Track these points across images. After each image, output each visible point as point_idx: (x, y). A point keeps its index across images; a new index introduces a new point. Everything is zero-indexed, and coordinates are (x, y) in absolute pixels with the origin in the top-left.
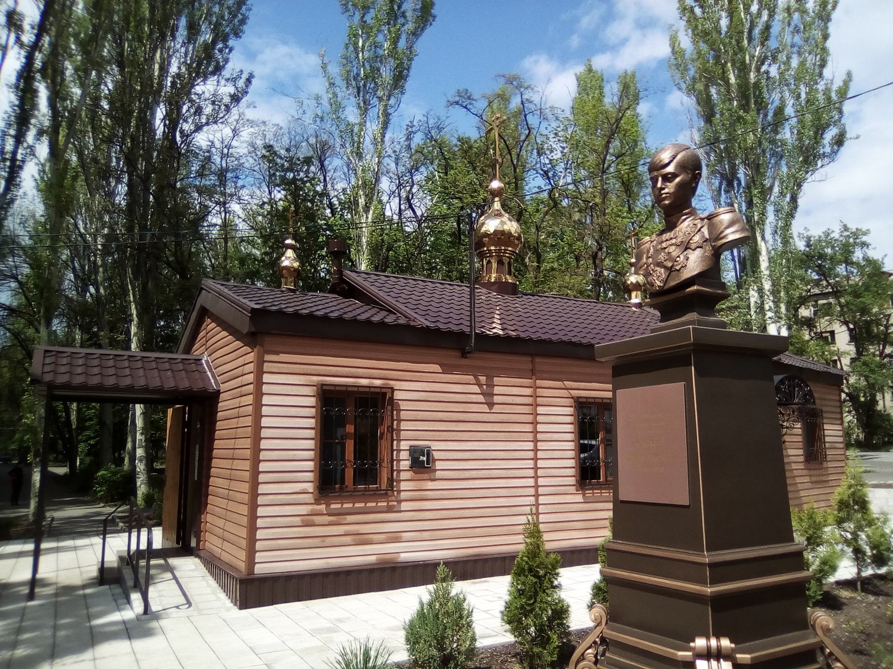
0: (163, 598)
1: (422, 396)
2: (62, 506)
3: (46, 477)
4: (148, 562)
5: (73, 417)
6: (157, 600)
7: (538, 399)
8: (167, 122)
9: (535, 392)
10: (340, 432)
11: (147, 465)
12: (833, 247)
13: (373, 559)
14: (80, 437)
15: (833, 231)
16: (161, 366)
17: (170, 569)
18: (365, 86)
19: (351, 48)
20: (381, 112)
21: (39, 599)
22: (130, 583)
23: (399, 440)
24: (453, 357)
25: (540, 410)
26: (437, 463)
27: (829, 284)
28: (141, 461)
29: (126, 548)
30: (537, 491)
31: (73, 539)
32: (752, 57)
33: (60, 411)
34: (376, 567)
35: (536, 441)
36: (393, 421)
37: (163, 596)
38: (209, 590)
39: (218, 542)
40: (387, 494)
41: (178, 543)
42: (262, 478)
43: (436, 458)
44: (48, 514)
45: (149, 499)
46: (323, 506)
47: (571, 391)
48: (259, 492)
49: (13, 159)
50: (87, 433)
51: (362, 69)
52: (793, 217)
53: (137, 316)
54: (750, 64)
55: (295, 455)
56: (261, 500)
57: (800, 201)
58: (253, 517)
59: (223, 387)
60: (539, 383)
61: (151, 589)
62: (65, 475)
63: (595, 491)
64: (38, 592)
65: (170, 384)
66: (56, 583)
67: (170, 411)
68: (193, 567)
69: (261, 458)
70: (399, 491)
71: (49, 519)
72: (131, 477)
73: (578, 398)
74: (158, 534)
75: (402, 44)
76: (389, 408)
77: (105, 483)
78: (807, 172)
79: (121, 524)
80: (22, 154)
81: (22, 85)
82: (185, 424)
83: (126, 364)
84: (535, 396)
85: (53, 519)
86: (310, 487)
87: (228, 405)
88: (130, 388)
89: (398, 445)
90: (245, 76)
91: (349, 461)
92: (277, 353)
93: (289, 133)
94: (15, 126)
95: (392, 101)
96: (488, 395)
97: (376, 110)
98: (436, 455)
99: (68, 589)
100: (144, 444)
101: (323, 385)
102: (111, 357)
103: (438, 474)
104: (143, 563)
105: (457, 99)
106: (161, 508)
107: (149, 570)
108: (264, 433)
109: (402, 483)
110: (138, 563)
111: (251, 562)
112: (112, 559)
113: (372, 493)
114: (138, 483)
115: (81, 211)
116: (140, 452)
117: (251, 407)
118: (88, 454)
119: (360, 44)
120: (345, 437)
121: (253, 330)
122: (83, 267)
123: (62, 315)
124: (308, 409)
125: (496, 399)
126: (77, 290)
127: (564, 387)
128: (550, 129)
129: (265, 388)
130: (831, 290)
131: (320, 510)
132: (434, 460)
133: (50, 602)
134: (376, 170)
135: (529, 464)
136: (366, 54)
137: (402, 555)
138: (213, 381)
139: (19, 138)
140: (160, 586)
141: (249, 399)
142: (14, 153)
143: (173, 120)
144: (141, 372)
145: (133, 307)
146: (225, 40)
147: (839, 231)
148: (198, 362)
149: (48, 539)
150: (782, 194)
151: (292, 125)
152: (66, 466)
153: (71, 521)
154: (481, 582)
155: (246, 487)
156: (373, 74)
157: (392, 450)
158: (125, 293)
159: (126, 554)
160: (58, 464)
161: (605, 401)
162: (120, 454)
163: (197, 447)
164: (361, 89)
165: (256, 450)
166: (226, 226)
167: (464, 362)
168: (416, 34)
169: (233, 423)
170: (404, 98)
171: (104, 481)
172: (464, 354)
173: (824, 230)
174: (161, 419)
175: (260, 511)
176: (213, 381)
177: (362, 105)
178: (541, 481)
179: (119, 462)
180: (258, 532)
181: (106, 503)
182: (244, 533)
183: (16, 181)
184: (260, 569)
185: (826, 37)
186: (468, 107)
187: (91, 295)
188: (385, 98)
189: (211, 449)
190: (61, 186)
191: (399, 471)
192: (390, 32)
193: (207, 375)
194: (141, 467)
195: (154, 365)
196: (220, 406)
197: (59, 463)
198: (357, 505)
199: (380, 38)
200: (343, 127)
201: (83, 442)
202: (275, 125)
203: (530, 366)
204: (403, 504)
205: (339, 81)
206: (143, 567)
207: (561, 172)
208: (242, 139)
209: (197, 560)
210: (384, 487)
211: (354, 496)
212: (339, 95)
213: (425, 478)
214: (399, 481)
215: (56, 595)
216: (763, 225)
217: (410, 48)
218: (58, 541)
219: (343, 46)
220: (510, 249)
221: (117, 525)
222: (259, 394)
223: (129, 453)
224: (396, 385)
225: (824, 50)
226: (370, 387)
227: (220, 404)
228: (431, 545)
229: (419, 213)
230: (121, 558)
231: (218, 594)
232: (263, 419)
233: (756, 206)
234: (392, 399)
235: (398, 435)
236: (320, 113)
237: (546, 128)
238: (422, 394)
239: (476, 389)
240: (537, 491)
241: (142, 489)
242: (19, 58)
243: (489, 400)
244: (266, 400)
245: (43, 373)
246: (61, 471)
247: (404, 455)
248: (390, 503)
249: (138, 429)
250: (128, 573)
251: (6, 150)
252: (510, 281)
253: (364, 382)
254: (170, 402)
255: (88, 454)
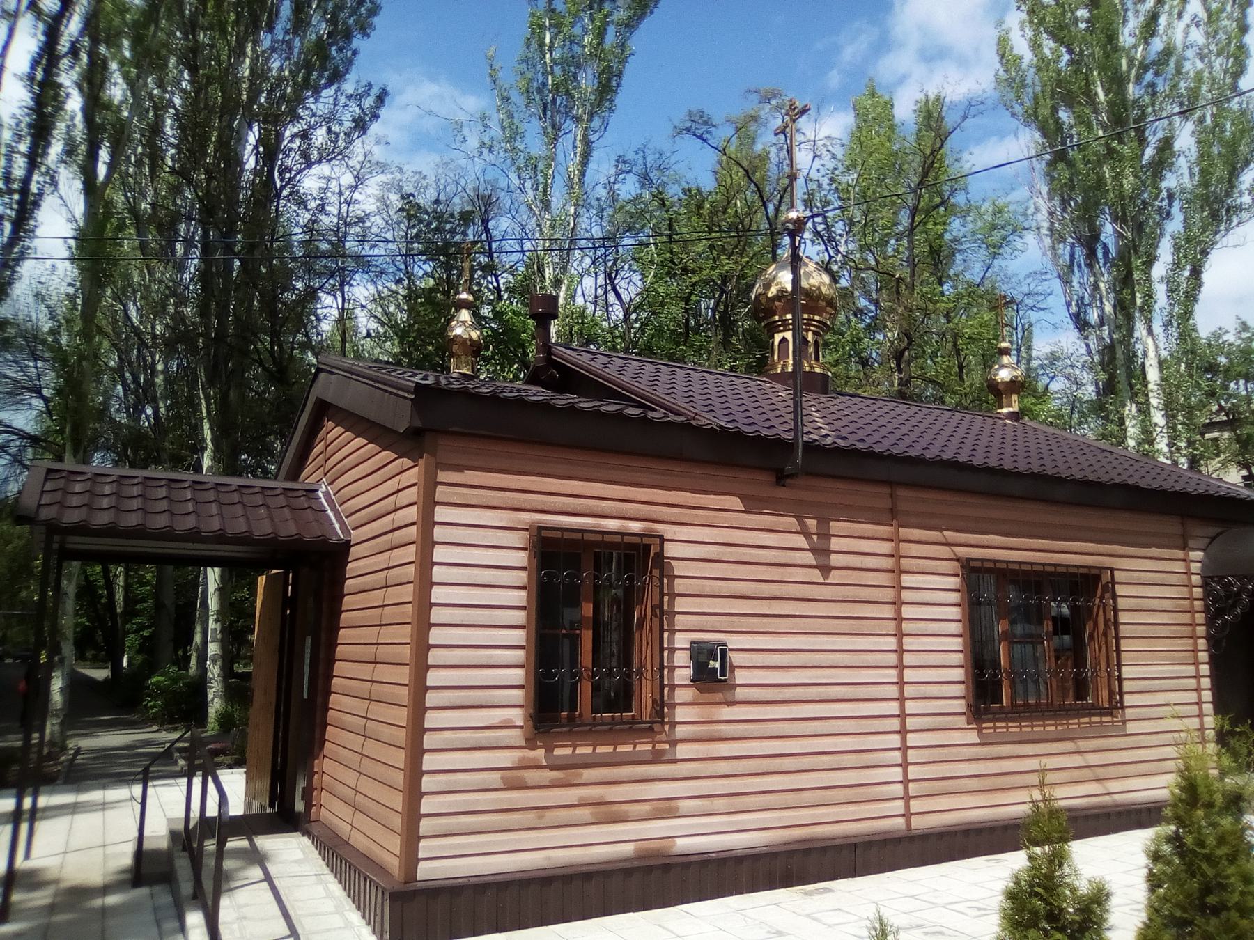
0: (245, 923)
1: (712, 551)
2: (92, 730)
3: (77, 686)
4: (221, 843)
5: (119, 596)
6: (235, 926)
7: (903, 561)
8: (261, 149)
9: (897, 548)
10: (568, 614)
11: (223, 668)
12: (1228, 356)
13: (628, 849)
14: (128, 626)
15: (1227, 332)
16: (248, 500)
17: (257, 858)
18: (554, 101)
19: (534, 45)
20: (578, 138)
21: (16, 921)
22: (186, 888)
23: (673, 632)
24: (761, 484)
25: (907, 580)
26: (738, 673)
27: (1221, 408)
28: (214, 662)
29: (182, 814)
30: (903, 724)
31: (104, 787)
32: (1131, 62)
33: (100, 587)
34: (636, 864)
35: (900, 635)
36: (662, 595)
37: (245, 918)
38: (329, 906)
39: (345, 811)
40: (651, 729)
41: (272, 805)
42: (431, 698)
43: (735, 663)
44: (71, 744)
45: (226, 721)
46: (540, 753)
47: (956, 549)
48: (426, 726)
49: (24, 191)
50: (139, 620)
51: (550, 77)
52: (1196, 300)
53: (212, 441)
54: (1129, 72)
55: (491, 656)
56: (429, 740)
57: (1206, 277)
58: (415, 772)
59: (355, 536)
60: (904, 532)
61: (225, 902)
62: (106, 680)
63: (998, 724)
64: (20, 902)
65: (263, 529)
66: (56, 881)
67: (262, 580)
68: (300, 855)
69: (430, 662)
70: (673, 725)
71: (72, 752)
72: (200, 685)
73: (968, 560)
74: (234, 782)
75: (610, 38)
76: (656, 572)
77: (161, 693)
78: (1216, 233)
79: (181, 762)
80: (38, 182)
81: (39, 75)
82: (287, 602)
83: (188, 494)
84: (896, 555)
85: (78, 751)
86: (517, 716)
87: (364, 567)
88: (194, 536)
89: (671, 640)
90: (375, 91)
91: (587, 669)
92: (460, 468)
93: (437, 181)
94: (29, 138)
95: (596, 123)
96: (821, 552)
97: (572, 135)
98: (736, 659)
99: (79, 894)
100: (219, 636)
101: (540, 528)
102: (163, 483)
103: (740, 693)
104: (210, 846)
105: (688, 124)
106: (244, 734)
107: (217, 851)
108: (437, 615)
109: (678, 710)
110: (201, 846)
111: (411, 857)
112: (158, 832)
113: (627, 726)
114: (210, 697)
115: (136, 298)
116: (213, 649)
117: (412, 568)
118: (140, 650)
119: (547, 40)
120: (576, 625)
121: (418, 424)
122: (136, 379)
123: (106, 448)
124: (514, 573)
125: (835, 560)
126: (128, 412)
127: (944, 541)
128: (823, 171)
129: (439, 533)
130: (1225, 418)
131: (536, 759)
132: (733, 668)
133: (31, 929)
134: (572, 224)
135: (889, 676)
136: (557, 54)
137: (679, 841)
138: (337, 526)
139: (34, 159)
140: (242, 896)
141: (410, 553)
142: (26, 181)
143: (270, 150)
144: (214, 508)
145: (206, 426)
146: (348, 36)
147: (1234, 332)
148: (312, 495)
149: (65, 787)
150: (1177, 265)
151: (440, 171)
152: (107, 668)
153: (106, 755)
154: (819, 892)
155: (401, 716)
156: (565, 88)
157: (662, 649)
158: (196, 408)
159: (181, 826)
160: (96, 665)
161: (1011, 566)
162: (185, 652)
163: (309, 640)
164: (549, 105)
165: (422, 647)
166: (344, 318)
167: (781, 493)
168: (630, 25)
169: (376, 597)
170: (614, 120)
171: (161, 690)
172: (781, 478)
173: (1213, 330)
174: (246, 599)
175: (429, 762)
176: (337, 526)
177: (550, 129)
178: (910, 707)
179: (184, 663)
180: (425, 800)
181: (162, 724)
182: (397, 801)
183: (28, 225)
184: (427, 871)
185: (1244, 29)
186: (705, 136)
187: (147, 417)
188: (585, 117)
189: (333, 644)
190: (101, 240)
191: (673, 687)
192: (592, 19)
193: (328, 516)
194: (214, 671)
195: (236, 497)
196: (351, 569)
197: (97, 663)
198: (600, 750)
199: (577, 30)
200: (521, 162)
201: (133, 633)
202: (416, 173)
203: (887, 503)
204: (680, 747)
205: (518, 99)
206: (210, 854)
207: (840, 235)
208: (369, 191)
209: (306, 841)
210: (646, 717)
211: (593, 732)
212: (516, 115)
213: (718, 700)
214: (673, 706)
215: (52, 909)
216: (1150, 312)
217: (623, 46)
218: (79, 790)
219: (522, 43)
220: (817, 318)
221: (176, 763)
222: (427, 544)
223: (197, 650)
224: (668, 531)
225: (1242, 48)
226: (623, 534)
227: (350, 566)
228: (729, 823)
229: (626, 298)
230: (173, 834)
231: (347, 914)
232: (435, 590)
233: (1139, 284)
234: (660, 555)
235: (671, 623)
236: (488, 142)
237: (818, 170)
238: (712, 548)
239: (801, 541)
240: (903, 724)
241: (215, 704)
242: (35, 35)
243: (823, 562)
244: (439, 554)
245: (39, 506)
246: (101, 674)
247: (682, 658)
248: (658, 746)
249: (210, 613)
250: (182, 864)
251: (13, 176)
252: (817, 370)
253: (612, 525)
254: (260, 566)
255: (139, 652)
